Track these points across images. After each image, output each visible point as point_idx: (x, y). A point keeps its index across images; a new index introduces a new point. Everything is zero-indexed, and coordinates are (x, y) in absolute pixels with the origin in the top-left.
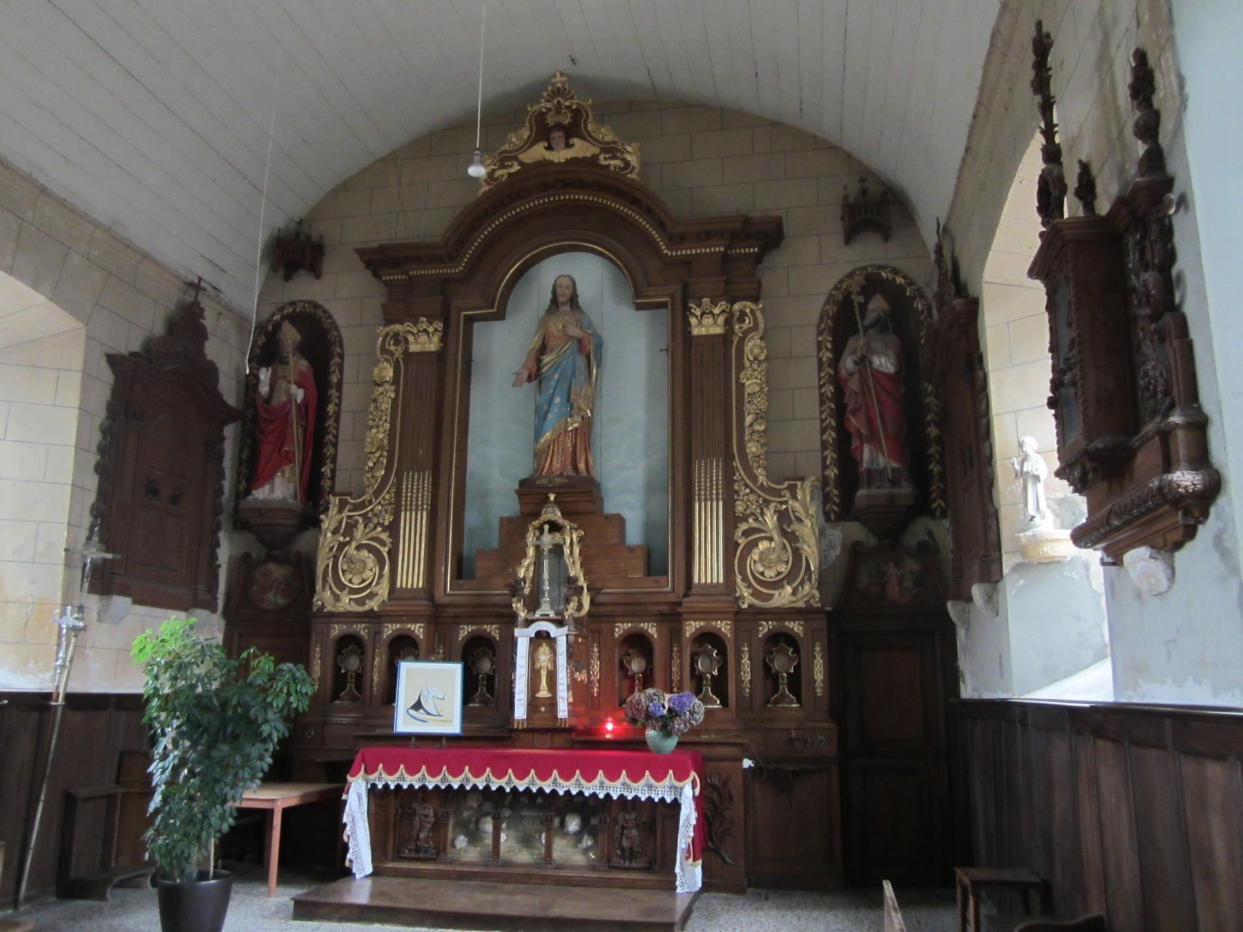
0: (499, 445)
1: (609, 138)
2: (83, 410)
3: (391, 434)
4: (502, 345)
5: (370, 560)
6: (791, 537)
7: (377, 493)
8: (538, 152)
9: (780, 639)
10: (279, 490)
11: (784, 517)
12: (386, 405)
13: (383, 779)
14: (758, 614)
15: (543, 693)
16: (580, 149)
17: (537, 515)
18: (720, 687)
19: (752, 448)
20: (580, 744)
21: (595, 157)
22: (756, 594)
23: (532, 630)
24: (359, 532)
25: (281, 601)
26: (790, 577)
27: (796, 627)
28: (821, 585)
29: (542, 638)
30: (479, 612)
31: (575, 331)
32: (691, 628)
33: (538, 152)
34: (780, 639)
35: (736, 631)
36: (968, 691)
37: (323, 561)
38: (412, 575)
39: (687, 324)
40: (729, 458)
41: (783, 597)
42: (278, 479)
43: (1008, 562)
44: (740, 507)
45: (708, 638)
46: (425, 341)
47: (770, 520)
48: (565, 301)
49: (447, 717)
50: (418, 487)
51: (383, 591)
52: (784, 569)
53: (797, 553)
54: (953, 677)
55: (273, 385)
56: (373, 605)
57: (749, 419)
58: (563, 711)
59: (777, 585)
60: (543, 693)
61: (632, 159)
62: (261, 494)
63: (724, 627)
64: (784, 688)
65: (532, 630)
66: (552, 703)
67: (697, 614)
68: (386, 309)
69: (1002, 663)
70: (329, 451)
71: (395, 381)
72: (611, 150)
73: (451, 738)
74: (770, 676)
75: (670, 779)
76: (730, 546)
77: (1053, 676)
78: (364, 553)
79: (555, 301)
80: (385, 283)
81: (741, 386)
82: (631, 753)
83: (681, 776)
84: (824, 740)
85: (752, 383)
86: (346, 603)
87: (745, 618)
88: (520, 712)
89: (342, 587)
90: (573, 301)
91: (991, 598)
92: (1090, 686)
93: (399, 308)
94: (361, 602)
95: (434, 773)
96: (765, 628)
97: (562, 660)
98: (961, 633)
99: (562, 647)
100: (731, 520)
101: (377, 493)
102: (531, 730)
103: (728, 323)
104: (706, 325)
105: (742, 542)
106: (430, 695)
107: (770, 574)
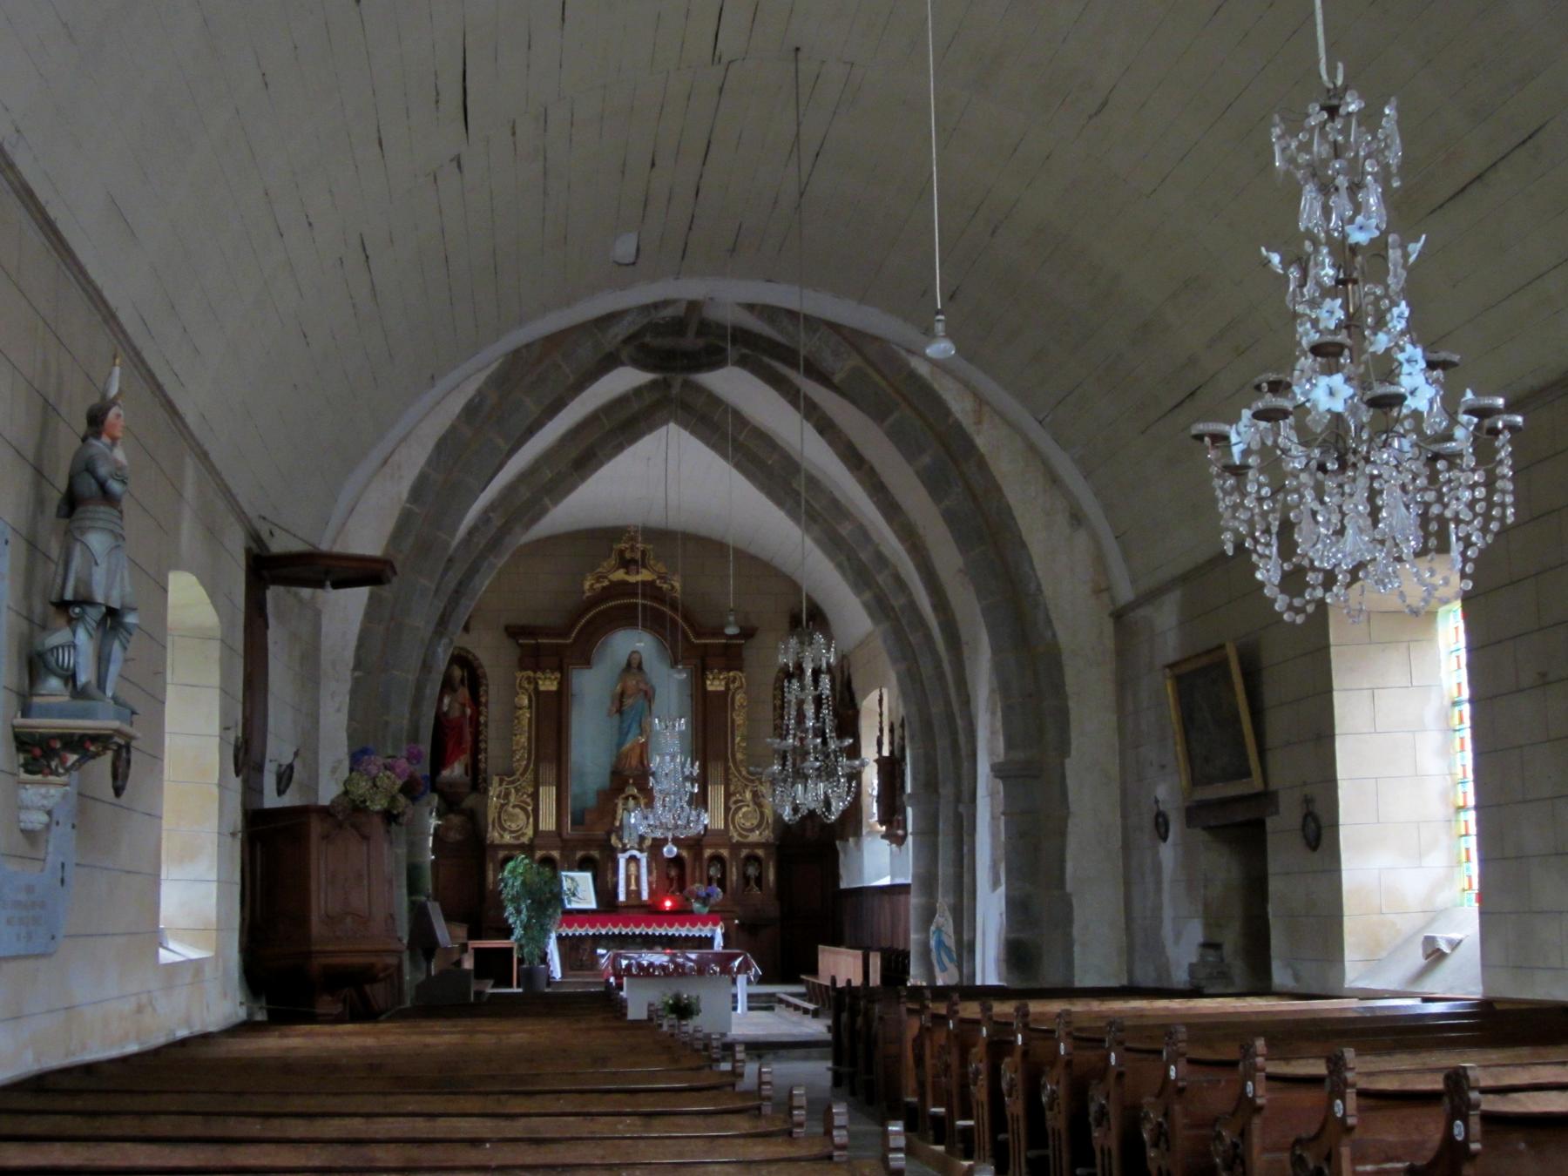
0: (590, 747)
1: (663, 570)
2: (225, 691)
3: (529, 739)
4: (592, 687)
5: (522, 815)
6: (760, 806)
7: (522, 775)
8: (620, 575)
9: (752, 858)
10: (455, 771)
11: (755, 794)
12: (525, 722)
13: (567, 931)
14: (740, 845)
15: (633, 887)
16: (644, 575)
17: (622, 790)
18: (722, 883)
19: (739, 756)
20: (652, 912)
21: (653, 582)
22: (740, 835)
23: (627, 855)
24: (512, 798)
25: (458, 837)
26: (759, 826)
27: (760, 852)
28: (774, 831)
29: (633, 858)
30: (587, 843)
31: (642, 686)
32: (708, 853)
33: (620, 575)
34: (752, 858)
35: (731, 854)
36: (843, 885)
37: (492, 814)
38: (548, 823)
39: (704, 684)
40: (726, 761)
41: (755, 837)
42: (456, 765)
43: (865, 831)
44: (732, 788)
45: (717, 859)
46: (549, 685)
47: (748, 795)
48: (633, 666)
49: (590, 903)
50: (548, 771)
51: (530, 832)
52: (755, 822)
53: (762, 814)
54: (836, 877)
55: (450, 705)
56: (525, 840)
57: (738, 739)
58: (645, 896)
59: (752, 830)
60: (633, 887)
61: (677, 585)
62: (446, 773)
63: (725, 853)
64: (752, 883)
65: (627, 855)
66: (638, 892)
67: (710, 846)
68: (521, 660)
69: (860, 871)
70: (482, 746)
71: (530, 707)
72: (662, 577)
73: (592, 911)
74: (746, 879)
75: (710, 926)
76: (727, 809)
77: (880, 877)
78: (517, 810)
79: (629, 664)
80: (521, 646)
81: (733, 721)
82: (682, 914)
83: (715, 924)
84: (773, 910)
85: (739, 720)
86: (507, 838)
87: (736, 847)
88: (622, 897)
89: (504, 829)
90: (640, 667)
91: (858, 845)
92: (886, 881)
93: (533, 659)
94: (517, 838)
95: (593, 926)
96: (744, 852)
97: (644, 871)
98: (842, 856)
99: (644, 862)
100: (728, 796)
101: (522, 775)
102: (627, 906)
103: (727, 685)
104: (715, 685)
105: (733, 807)
106: (581, 890)
107: (748, 825)
